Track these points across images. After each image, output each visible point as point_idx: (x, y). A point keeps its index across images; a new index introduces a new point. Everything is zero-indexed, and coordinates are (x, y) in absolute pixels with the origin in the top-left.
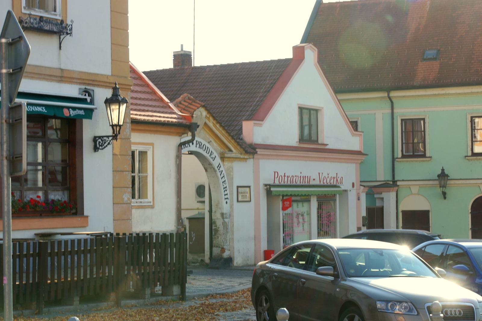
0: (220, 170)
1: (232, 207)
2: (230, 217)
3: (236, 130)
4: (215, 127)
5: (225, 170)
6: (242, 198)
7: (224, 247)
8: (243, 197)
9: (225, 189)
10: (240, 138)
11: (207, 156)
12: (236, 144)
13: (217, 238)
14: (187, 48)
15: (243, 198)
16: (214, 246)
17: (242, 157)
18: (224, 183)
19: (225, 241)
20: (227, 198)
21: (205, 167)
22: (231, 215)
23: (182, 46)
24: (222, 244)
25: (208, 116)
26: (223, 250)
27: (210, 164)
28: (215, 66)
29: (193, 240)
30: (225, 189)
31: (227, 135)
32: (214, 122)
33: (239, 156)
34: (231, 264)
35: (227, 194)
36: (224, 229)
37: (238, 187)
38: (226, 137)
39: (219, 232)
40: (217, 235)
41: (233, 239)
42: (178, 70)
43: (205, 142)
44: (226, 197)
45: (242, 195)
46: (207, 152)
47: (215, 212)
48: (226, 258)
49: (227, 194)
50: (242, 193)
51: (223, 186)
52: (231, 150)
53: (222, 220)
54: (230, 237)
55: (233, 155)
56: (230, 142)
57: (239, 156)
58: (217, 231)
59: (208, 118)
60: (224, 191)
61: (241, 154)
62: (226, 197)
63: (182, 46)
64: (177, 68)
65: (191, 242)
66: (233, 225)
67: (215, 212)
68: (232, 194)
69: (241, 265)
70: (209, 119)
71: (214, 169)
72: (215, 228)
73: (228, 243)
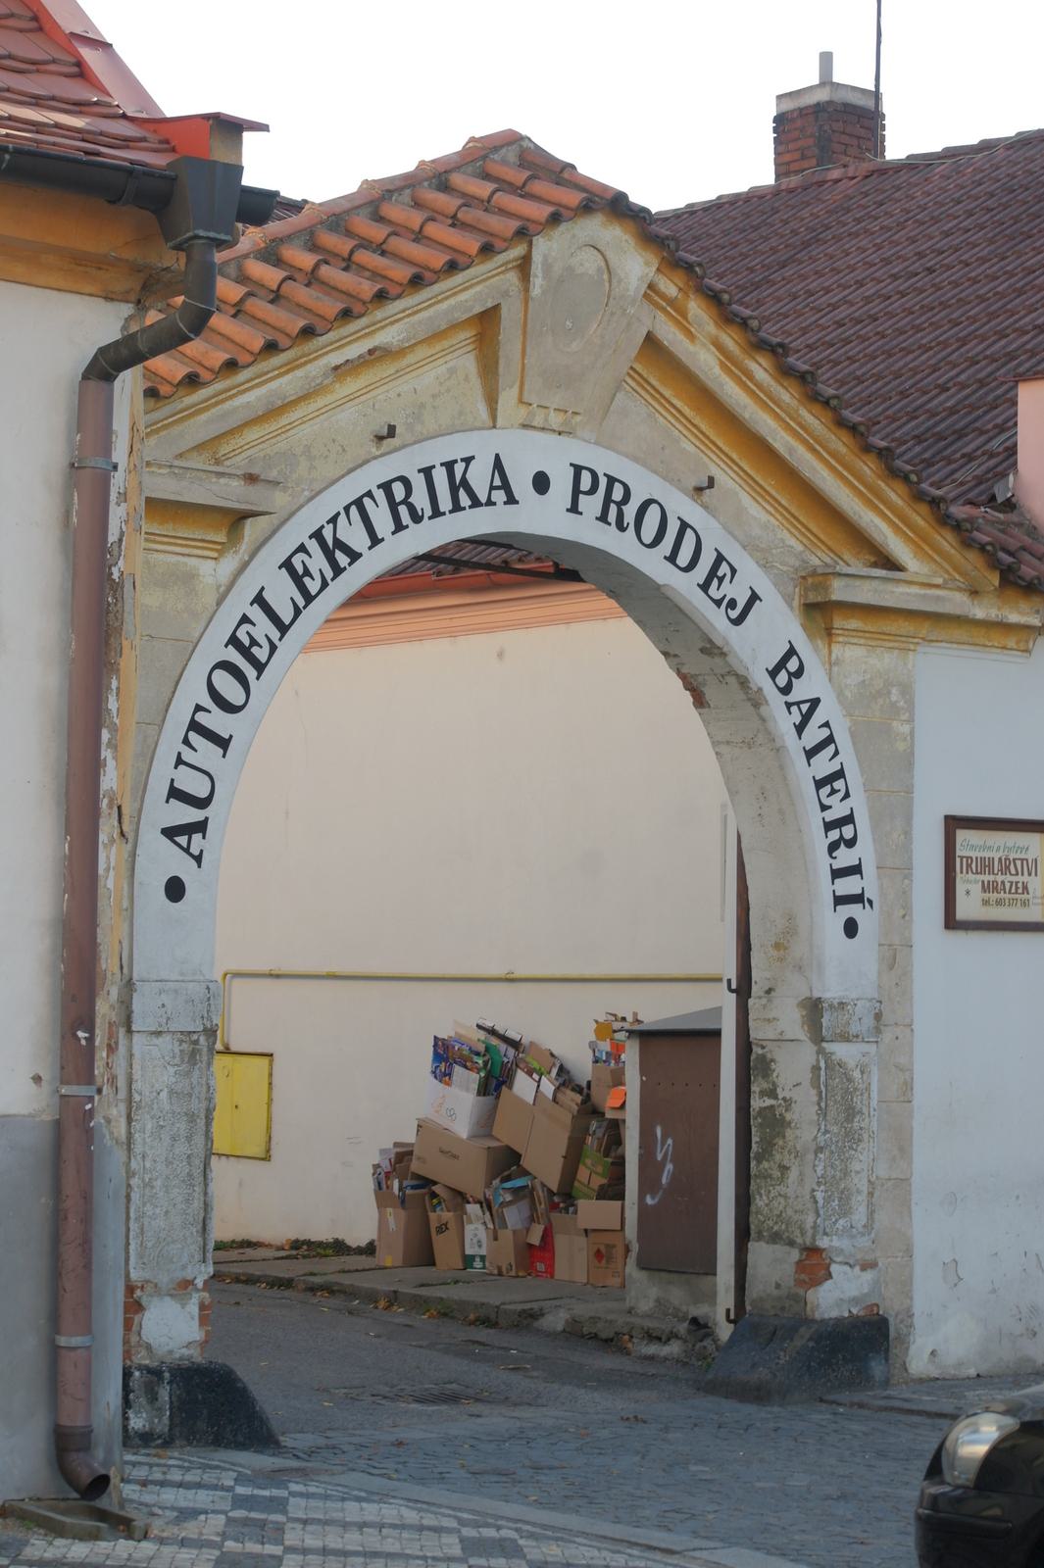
0: (792, 698)
1: (895, 957)
2: (878, 1031)
3: (992, 455)
4: (743, 378)
5: (840, 695)
6: (986, 903)
7: (823, 1243)
8: (994, 896)
9: (834, 835)
10: (993, 498)
11: (685, 586)
12: (920, 517)
13: (776, 1174)
14: (854, 74)
15: (999, 903)
16: (760, 1237)
17: (979, 612)
18: (827, 789)
19: (828, 1200)
20: (858, 899)
21: (684, 670)
22: (887, 1017)
23: (826, 60)
24: (810, 1220)
25: (669, 287)
26: (814, 1264)
27: (712, 649)
28: (986, 146)
29: (664, 1180)
30: (834, 835)
31: (840, 442)
32: (730, 340)
33: (957, 602)
34: (877, 1369)
35: (856, 870)
36: (823, 1112)
37: (954, 824)
38: (834, 454)
39: (789, 1133)
40: (778, 1157)
41: (904, 1183)
42: (791, 191)
43: (655, 479)
44: (848, 886)
45: (987, 878)
46: (672, 559)
47: (769, 991)
48: (839, 1321)
49: (856, 870)
50: (986, 866)
51: (824, 808)
52: (889, 563)
53: (807, 1054)
54: (882, 1170)
55: (850, 570)
56: (873, 499)
57: (957, 602)
58: (776, 1123)
59: (671, 302)
60: (833, 847)
61: (974, 593)
62: (848, 886)
63: (826, 60)
64: (794, 181)
65: (653, 1198)
66: (908, 1087)
67: (769, 991)
68: (900, 869)
69: (972, 1372)
70: (676, 311)
71: (744, 682)
72: (769, 1102)
73: (860, 1216)
